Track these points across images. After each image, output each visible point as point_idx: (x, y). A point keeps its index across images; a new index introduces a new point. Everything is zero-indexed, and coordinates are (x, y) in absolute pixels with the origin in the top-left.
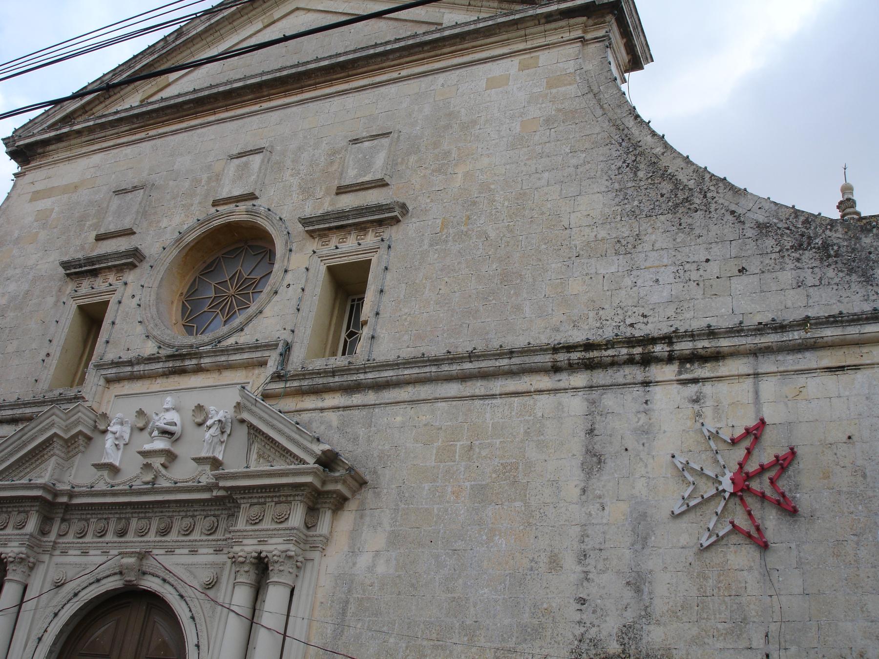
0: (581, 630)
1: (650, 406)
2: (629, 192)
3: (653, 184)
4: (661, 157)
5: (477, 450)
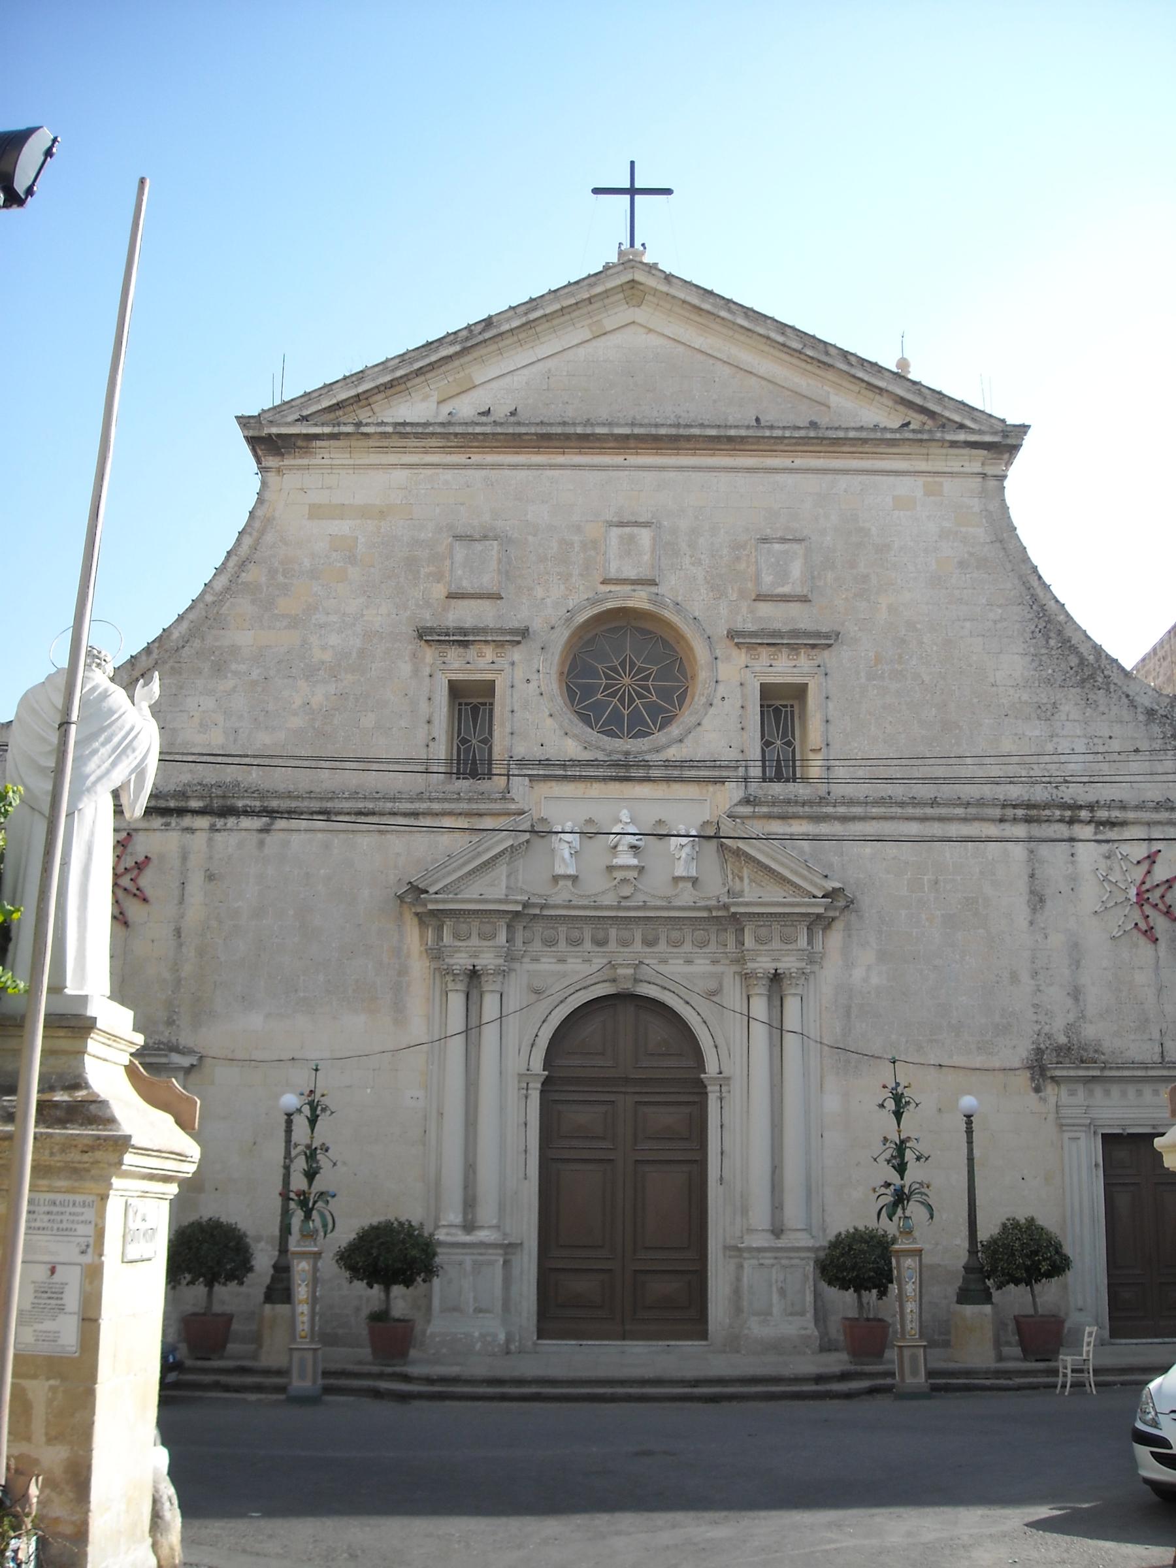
0: (1037, 1028)
1: (1075, 858)
2: (1043, 658)
3: (1063, 655)
4: (1065, 626)
5: (942, 884)
